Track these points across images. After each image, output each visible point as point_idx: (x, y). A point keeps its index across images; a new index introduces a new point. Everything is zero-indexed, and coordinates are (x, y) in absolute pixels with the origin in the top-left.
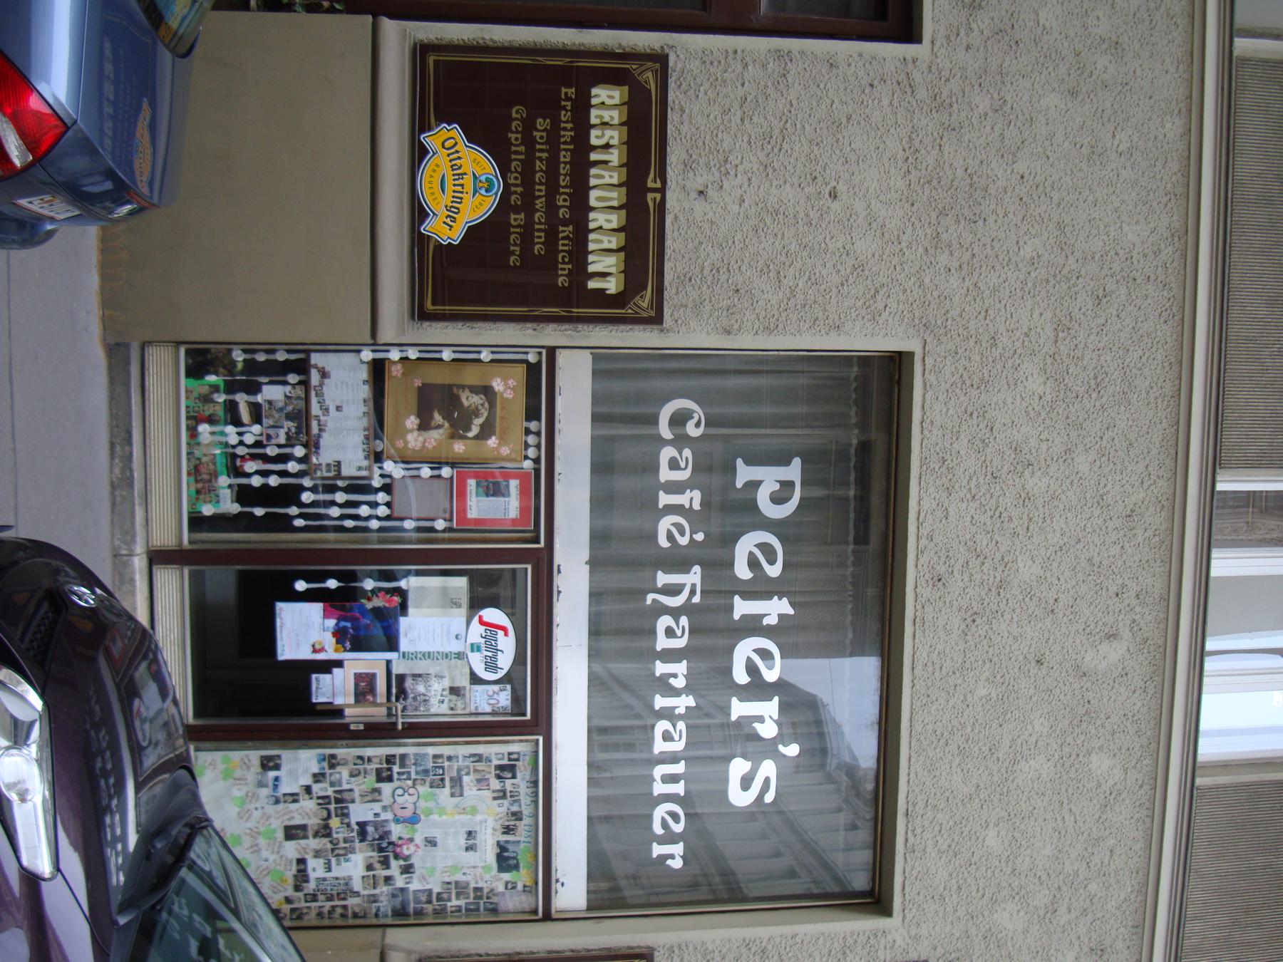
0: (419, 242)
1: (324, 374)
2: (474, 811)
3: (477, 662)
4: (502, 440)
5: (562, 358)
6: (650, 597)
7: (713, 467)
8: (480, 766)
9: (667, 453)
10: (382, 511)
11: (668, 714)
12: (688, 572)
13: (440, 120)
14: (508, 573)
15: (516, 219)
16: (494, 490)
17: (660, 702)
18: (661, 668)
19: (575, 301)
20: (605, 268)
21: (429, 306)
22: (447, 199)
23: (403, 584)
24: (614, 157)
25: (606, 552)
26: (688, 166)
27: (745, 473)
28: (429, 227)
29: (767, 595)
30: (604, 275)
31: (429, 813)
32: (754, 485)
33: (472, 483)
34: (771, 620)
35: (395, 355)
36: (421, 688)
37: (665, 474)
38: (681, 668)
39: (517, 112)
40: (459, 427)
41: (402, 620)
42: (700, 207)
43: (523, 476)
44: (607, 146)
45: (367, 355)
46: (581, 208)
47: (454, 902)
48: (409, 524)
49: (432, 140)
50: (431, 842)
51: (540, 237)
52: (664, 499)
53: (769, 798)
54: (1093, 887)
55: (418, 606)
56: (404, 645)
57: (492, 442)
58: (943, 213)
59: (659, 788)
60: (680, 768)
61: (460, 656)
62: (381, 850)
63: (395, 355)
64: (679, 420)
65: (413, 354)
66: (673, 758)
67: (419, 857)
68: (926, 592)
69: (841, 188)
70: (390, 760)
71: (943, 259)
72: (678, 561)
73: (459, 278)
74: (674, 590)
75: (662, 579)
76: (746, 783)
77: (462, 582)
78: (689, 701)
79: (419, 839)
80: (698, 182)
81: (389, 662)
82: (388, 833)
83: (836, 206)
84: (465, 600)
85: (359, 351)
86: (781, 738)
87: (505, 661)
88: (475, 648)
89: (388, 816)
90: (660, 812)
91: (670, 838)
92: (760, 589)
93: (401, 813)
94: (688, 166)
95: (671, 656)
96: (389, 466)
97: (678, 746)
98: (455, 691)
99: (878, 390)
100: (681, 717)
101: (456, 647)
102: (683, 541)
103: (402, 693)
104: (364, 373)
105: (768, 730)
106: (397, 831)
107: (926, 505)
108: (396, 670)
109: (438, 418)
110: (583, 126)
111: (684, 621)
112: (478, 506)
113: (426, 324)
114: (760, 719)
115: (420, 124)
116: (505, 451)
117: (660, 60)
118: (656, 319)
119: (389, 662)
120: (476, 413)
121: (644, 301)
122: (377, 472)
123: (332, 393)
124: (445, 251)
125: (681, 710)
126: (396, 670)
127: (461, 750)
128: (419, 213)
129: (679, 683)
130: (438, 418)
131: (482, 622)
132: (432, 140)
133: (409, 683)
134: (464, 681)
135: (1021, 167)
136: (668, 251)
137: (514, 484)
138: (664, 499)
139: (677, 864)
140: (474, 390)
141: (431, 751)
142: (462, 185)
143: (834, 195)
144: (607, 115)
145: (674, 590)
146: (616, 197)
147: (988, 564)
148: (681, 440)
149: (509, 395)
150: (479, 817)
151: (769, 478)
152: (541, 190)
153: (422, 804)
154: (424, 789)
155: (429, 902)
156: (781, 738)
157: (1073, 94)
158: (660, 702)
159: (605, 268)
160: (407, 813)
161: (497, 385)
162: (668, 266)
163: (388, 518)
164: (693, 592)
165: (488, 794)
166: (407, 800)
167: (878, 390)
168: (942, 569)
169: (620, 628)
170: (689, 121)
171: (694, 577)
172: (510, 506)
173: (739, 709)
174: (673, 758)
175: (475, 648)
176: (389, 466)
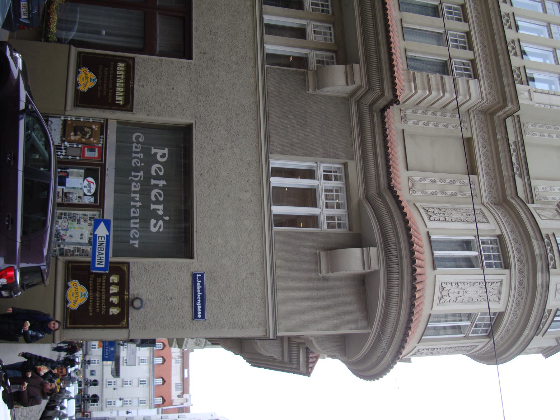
0: (77, 91)
1: (52, 122)
2: (83, 228)
3: (86, 190)
4: (94, 139)
5: (110, 121)
6: (130, 178)
7: (146, 151)
8: (85, 217)
9: (135, 145)
10: (64, 154)
11: (135, 207)
12: (140, 172)
13: (83, 66)
14: (95, 171)
15: (100, 88)
16: (92, 150)
17: (132, 203)
18: (133, 195)
19: (113, 106)
20: (120, 98)
21: (78, 104)
22: (74, 298)
23: (68, 170)
24: (122, 77)
25: (118, 171)
26: (139, 80)
27: (154, 151)
28: (79, 88)
29: (160, 180)
30: (119, 101)
31: (71, 228)
32: (156, 154)
33: (86, 149)
34: (161, 185)
35: (69, 119)
36: (71, 196)
37: (134, 149)
38: (138, 195)
39: (101, 66)
40: (84, 134)
41: (67, 179)
42: (142, 89)
43: (99, 147)
44: (121, 75)
45: (63, 118)
46: (115, 87)
47: (76, 253)
48: (70, 157)
49: (81, 70)
50: (71, 236)
51: (105, 92)
52: (134, 155)
53: (161, 230)
54: (249, 256)
55: (71, 176)
56: (67, 185)
57: (92, 139)
58: (199, 94)
59: (132, 225)
60: (137, 221)
61: (81, 189)
62: (57, 237)
63: (69, 119)
64: (138, 138)
65: (74, 119)
66: (135, 218)
67: (68, 240)
68: (198, 177)
69: (175, 87)
70: (61, 214)
71: (199, 104)
72: (137, 170)
73: (85, 99)
74: (136, 176)
75: (133, 174)
76: (155, 226)
77: (82, 171)
78: (140, 204)
79: (68, 235)
80: (142, 83)
81: (63, 189)
82: (60, 233)
83: (173, 91)
84: (83, 175)
85: (60, 117)
86: (165, 215)
87: (93, 191)
88: (85, 187)
89: (60, 228)
90: (132, 232)
91: (135, 239)
92: (158, 178)
93: (64, 228)
94: (139, 80)
95: (135, 192)
96: (66, 143)
97: (137, 215)
98: (80, 197)
99: (186, 131)
100: (138, 208)
101: (80, 186)
102: (139, 165)
103: (66, 197)
104: (61, 122)
105: (160, 213)
106: (62, 232)
107: (197, 157)
108: (65, 191)
109: (79, 133)
110: (116, 70)
111: (139, 184)
112: (88, 154)
113: (78, 108)
114: (159, 210)
115: (79, 66)
116: (95, 142)
117: (133, 59)
118: (131, 110)
119: (63, 189)
120: (88, 132)
121: (129, 106)
122: (63, 145)
123: (53, 126)
124: (73, 311)
125: (138, 206)
126: (65, 191)
127: (80, 213)
128: (77, 85)
129: (137, 199)
130: (79, 133)
131: (87, 181)
132: (81, 70)
133: (67, 195)
134: (82, 195)
135: (216, 86)
136: (135, 97)
137: (97, 149)
138: (134, 155)
139: (137, 246)
140: (88, 128)
141: (73, 212)
142: (87, 80)
143: (173, 89)
144: (121, 68)
145: (136, 176)
146: (122, 85)
147: (214, 172)
148: (138, 143)
149: (96, 129)
150: (84, 230)
151: (160, 152)
152: (105, 82)
153: (69, 226)
154: (70, 222)
155: (70, 252)
156: (165, 215)
157: (228, 72)
158: (132, 203)
159: (120, 98)
160: (65, 228)
161: (94, 127)
162: (134, 100)
163: (65, 155)
164: (141, 178)
165: (87, 224)
166: (65, 224)
167: (186, 131)
168: (202, 172)
169: (122, 188)
170: (139, 72)
171: (141, 174)
172: (96, 154)
173: (153, 207)
174: (135, 218)
175: (85, 187)
176: (66, 143)
